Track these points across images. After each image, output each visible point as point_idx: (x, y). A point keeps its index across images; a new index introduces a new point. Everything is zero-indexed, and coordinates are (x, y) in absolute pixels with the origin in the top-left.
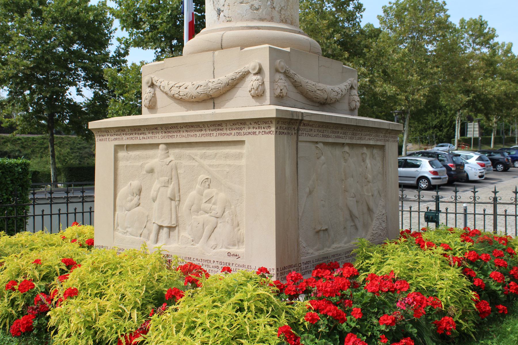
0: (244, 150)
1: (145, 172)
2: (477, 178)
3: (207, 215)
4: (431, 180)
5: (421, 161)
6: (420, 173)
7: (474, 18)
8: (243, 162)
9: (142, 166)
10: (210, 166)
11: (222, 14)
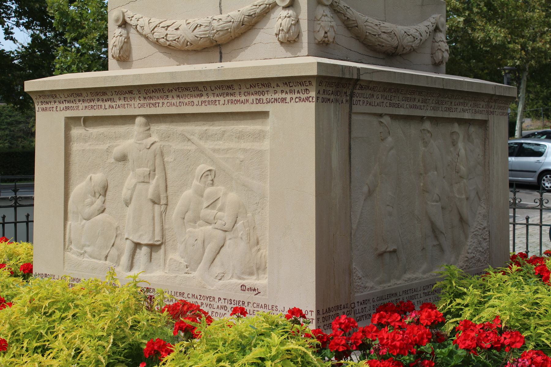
0: (267, 126)
1: (113, 160)
3: (209, 227)
5: (545, 146)
6: (543, 164)
8: (266, 145)
10: (214, 150)
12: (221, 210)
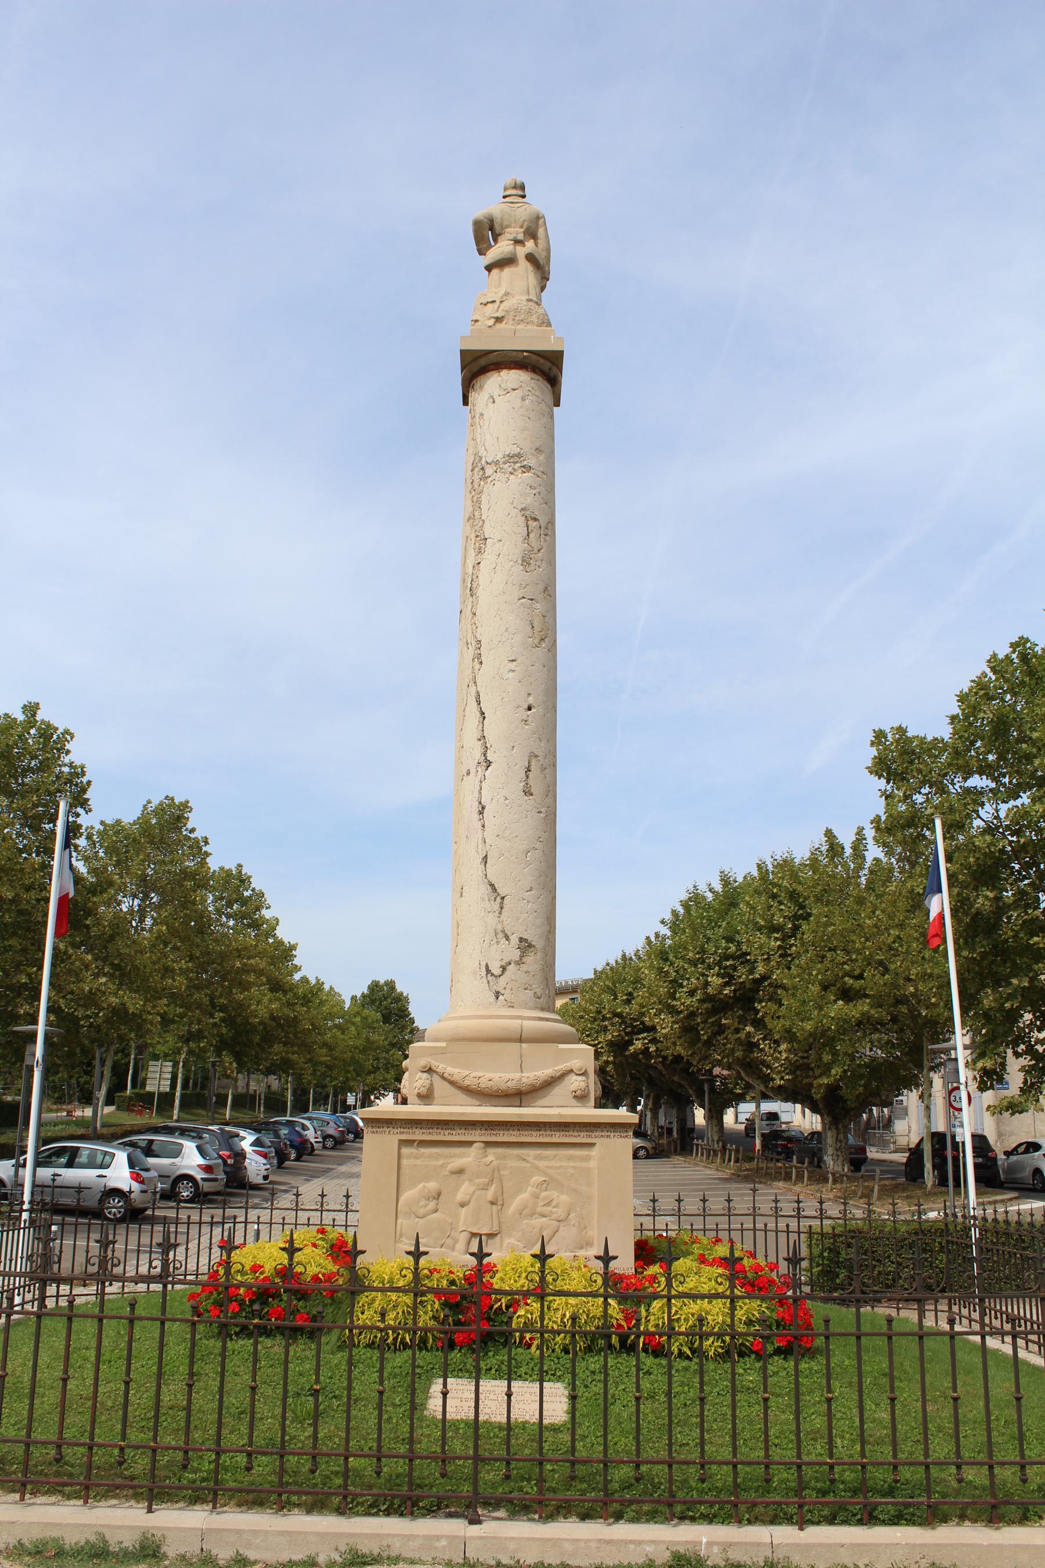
0: (594, 1152)
1: (447, 1173)
2: (259, 1180)
4: (201, 1182)
5: (182, 1145)
7: (227, 867)
9: (442, 1166)
10: (547, 1167)
11: (501, 997)
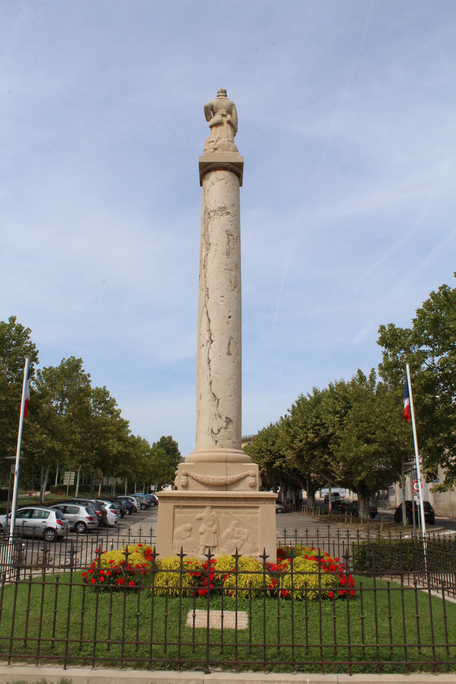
0: (259, 510)
2: (113, 523)
3: (237, 540)
4: (87, 524)
6: (78, 518)
8: (258, 515)
9: (193, 517)
10: (239, 517)
11: (218, 443)
12: (242, 534)
